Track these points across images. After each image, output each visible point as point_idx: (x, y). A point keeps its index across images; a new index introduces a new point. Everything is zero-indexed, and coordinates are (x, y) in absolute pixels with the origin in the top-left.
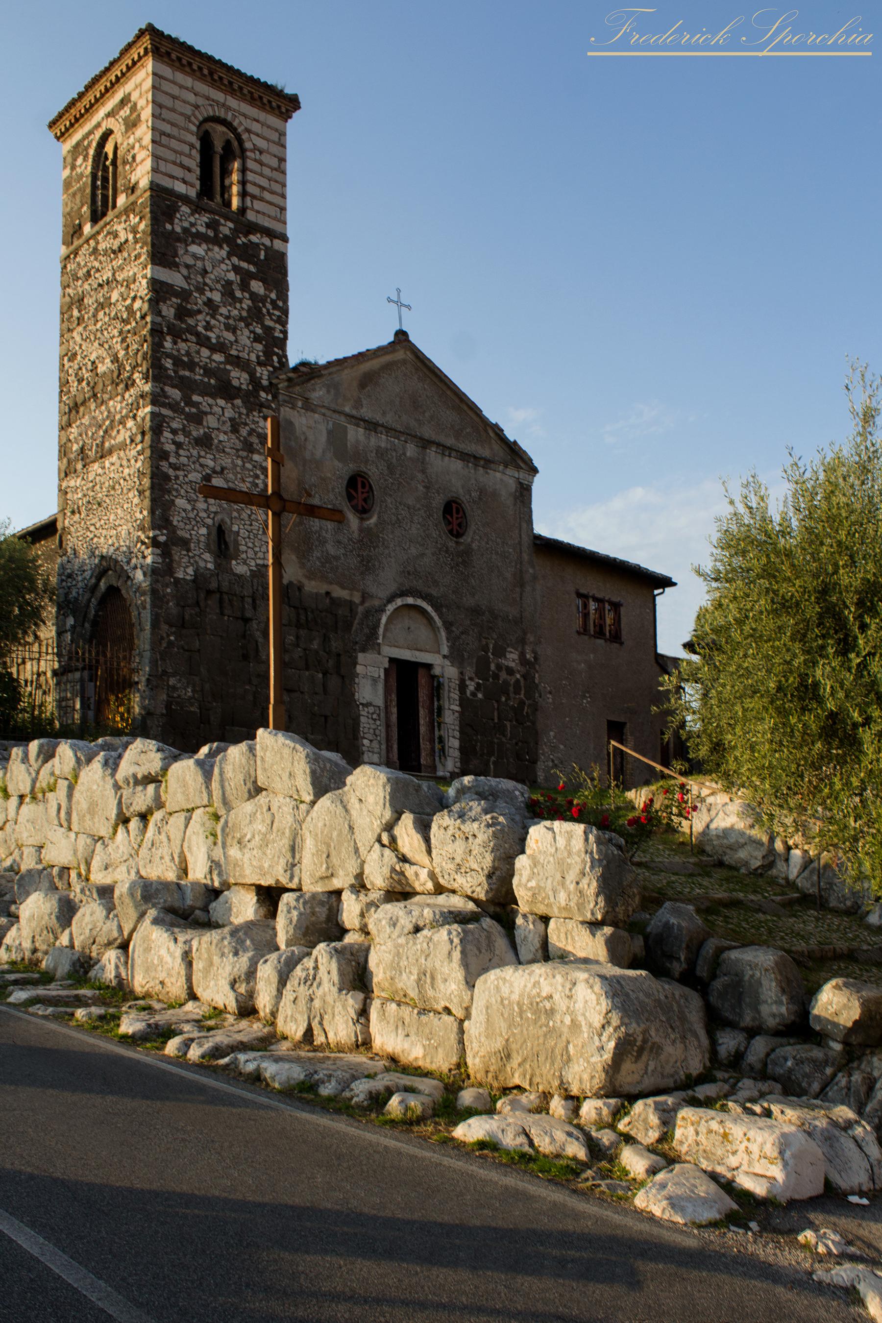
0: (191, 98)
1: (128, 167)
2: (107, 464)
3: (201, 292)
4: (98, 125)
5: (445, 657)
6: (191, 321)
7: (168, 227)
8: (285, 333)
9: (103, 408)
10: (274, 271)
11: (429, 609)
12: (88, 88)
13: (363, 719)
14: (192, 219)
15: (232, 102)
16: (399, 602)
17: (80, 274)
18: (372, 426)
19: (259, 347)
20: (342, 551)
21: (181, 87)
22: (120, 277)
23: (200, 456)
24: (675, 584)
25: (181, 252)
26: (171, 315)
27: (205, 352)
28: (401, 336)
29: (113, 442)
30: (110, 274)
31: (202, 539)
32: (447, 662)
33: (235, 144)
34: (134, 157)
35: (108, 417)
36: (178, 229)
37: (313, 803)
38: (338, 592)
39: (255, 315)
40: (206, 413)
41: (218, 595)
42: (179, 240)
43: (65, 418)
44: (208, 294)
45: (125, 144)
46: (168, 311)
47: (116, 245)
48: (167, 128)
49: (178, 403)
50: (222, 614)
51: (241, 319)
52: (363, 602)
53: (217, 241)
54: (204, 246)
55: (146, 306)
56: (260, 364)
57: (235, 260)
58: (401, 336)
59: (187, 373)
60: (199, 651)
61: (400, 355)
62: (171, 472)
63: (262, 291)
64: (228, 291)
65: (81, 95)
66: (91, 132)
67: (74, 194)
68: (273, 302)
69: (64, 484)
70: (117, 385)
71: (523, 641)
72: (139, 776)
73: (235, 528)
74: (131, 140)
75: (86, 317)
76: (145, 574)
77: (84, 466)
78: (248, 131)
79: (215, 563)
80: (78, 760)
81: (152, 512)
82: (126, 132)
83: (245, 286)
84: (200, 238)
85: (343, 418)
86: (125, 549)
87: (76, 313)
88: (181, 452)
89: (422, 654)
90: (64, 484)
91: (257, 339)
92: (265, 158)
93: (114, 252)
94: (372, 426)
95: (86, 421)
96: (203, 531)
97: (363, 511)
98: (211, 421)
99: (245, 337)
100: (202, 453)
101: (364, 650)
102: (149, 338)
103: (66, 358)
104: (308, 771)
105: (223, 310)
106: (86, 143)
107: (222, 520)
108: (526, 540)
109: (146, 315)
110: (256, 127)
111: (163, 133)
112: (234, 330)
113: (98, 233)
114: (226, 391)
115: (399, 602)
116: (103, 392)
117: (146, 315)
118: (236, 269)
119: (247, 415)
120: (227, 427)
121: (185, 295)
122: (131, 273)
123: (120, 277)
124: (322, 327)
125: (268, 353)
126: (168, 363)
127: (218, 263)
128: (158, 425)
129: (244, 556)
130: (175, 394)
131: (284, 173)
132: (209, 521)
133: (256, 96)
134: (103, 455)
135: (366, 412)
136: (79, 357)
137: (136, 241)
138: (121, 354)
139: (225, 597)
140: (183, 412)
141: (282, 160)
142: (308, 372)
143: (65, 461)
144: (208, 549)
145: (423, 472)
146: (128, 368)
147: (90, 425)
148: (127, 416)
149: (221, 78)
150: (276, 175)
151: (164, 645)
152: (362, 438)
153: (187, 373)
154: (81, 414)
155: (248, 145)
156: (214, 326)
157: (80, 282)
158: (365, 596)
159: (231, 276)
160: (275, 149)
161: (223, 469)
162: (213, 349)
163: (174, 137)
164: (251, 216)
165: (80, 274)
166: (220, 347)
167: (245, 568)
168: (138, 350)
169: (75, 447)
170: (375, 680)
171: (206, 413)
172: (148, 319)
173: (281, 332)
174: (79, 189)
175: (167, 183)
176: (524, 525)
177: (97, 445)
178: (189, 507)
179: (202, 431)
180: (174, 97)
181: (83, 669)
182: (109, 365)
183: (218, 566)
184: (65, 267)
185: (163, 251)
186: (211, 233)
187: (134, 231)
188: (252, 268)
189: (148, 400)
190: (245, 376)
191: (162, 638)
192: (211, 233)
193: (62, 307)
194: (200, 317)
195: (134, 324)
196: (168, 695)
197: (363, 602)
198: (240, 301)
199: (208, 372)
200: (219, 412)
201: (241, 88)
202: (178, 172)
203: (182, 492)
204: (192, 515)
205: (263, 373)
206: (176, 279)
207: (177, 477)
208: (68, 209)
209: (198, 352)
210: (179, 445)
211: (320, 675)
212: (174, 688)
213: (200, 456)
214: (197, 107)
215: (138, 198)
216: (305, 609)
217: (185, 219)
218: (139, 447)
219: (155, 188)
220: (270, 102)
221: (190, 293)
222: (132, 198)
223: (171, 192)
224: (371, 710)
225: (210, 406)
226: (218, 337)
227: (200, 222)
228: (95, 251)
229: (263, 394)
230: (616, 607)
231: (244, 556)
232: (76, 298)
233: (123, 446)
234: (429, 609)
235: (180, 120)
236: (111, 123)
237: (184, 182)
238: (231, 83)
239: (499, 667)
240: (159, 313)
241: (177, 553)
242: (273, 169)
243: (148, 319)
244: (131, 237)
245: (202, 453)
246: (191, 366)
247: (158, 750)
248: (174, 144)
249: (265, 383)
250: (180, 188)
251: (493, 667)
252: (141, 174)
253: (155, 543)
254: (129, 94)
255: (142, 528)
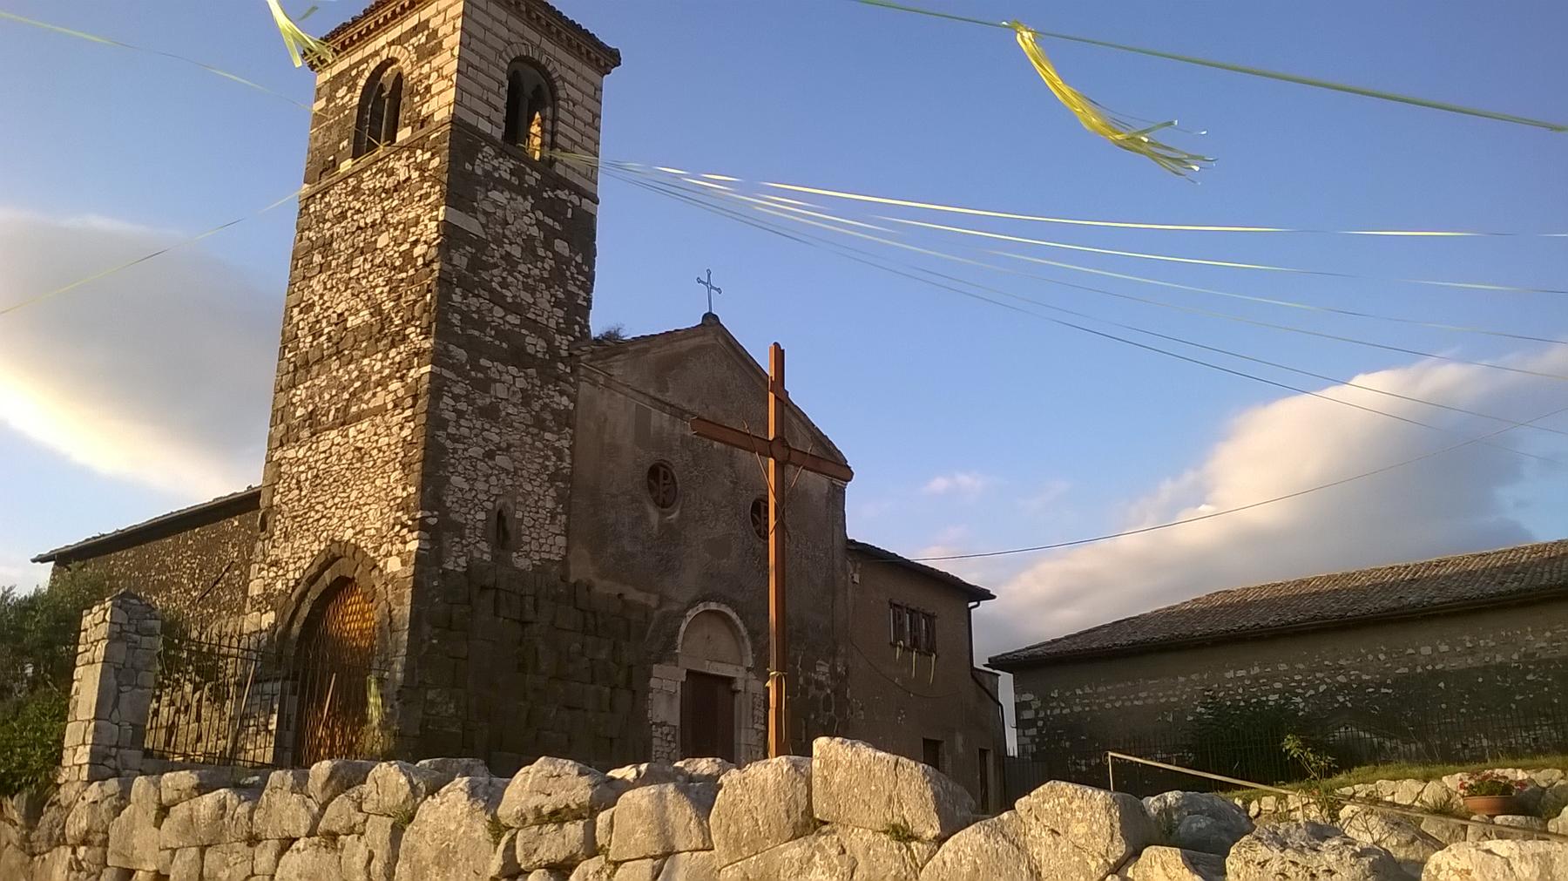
0: (504, 32)
1: (417, 99)
2: (352, 432)
3: (500, 245)
4: (377, 53)
5: (748, 669)
6: (484, 275)
7: (468, 166)
8: (589, 301)
9: (352, 366)
10: (582, 232)
11: (734, 616)
12: (367, 13)
13: (655, 741)
14: (495, 163)
15: (548, 46)
16: (701, 607)
17: (329, 215)
18: (678, 413)
19: (560, 313)
20: (639, 548)
21: (494, 19)
22: (393, 219)
23: (483, 430)
24: (993, 597)
25: (480, 197)
26: (463, 263)
27: (498, 312)
28: (710, 319)
29: (364, 406)
30: (378, 216)
31: (479, 525)
32: (751, 676)
33: (546, 90)
34: (428, 88)
35: (358, 378)
36: (479, 172)
37: (940, 840)
38: (633, 595)
39: (557, 276)
40: (495, 381)
41: (492, 593)
42: (479, 183)
43: (286, 378)
44: (508, 248)
45: (416, 74)
46: (460, 260)
47: (390, 183)
48: (476, 60)
49: (463, 366)
50: (496, 614)
51: (542, 280)
52: (659, 607)
53: (522, 191)
54: (507, 194)
55: (433, 252)
56: (559, 331)
57: (540, 214)
58: (710, 319)
59: (476, 333)
60: (467, 658)
61: (709, 340)
62: (448, 444)
63: (566, 253)
64: (529, 246)
65: (355, 21)
66: (365, 60)
67: (329, 128)
68: (578, 266)
69: (277, 455)
70: (378, 340)
71: (833, 653)
72: (545, 811)
73: (519, 515)
74: (426, 69)
75: (334, 263)
76: (404, 563)
77: (313, 434)
78: (564, 80)
79: (492, 553)
80: (414, 788)
81: (422, 489)
82: (419, 60)
83: (548, 245)
84: (502, 185)
85: (647, 401)
86: (373, 532)
87: (317, 259)
88: (462, 422)
89: (719, 665)
90: (277, 455)
91: (558, 304)
92: (578, 110)
93: (386, 191)
94: (678, 413)
95: (322, 381)
96: (482, 516)
97: (663, 505)
98: (500, 390)
99: (544, 299)
100: (487, 426)
101: (659, 661)
102: (434, 288)
103: (296, 310)
104: (929, 794)
105: (522, 268)
106: (354, 73)
107: (504, 504)
108: (838, 543)
109: (432, 261)
110: (570, 76)
111: (470, 65)
112: (532, 290)
113: (363, 170)
114: (518, 357)
115: (701, 607)
116: (352, 348)
117: (432, 261)
118: (539, 224)
119: (541, 387)
120: (517, 399)
121: (481, 245)
122: (412, 215)
123: (393, 219)
124: (633, 295)
125: (570, 322)
126: (456, 319)
127: (523, 217)
128: (437, 386)
129: (527, 548)
130: (461, 354)
131: (598, 129)
132: (489, 505)
133: (574, 43)
134: (345, 420)
135: (669, 397)
136: (317, 309)
137: (423, 179)
138: (388, 305)
139: (502, 594)
140: (466, 376)
141: (597, 116)
142: (612, 344)
143: (282, 427)
144: (485, 538)
145: (731, 466)
146: (397, 321)
147: (327, 387)
148: (390, 377)
149: (538, 18)
150: (589, 130)
151: (425, 649)
152: (666, 424)
153: (476, 333)
154: (314, 373)
155: (562, 94)
156: (511, 284)
157: (328, 225)
158: (663, 600)
159: (534, 231)
160: (589, 103)
161: (509, 446)
162: (508, 309)
163: (481, 71)
164: (559, 169)
165: (329, 215)
166: (516, 308)
167: (528, 562)
168: (416, 302)
169: (300, 412)
170: (671, 696)
171: (495, 381)
172: (436, 266)
173: (585, 299)
174: (338, 122)
175: (471, 119)
176: (837, 529)
177: (337, 410)
178: (466, 487)
179: (488, 401)
180: (486, 29)
181: (286, 679)
182: (367, 318)
183: (495, 558)
184: (307, 207)
185: (459, 190)
186: (515, 180)
187: (421, 168)
188: (557, 227)
189: (427, 357)
190: (542, 343)
191: (423, 641)
192: (515, 180)
193: (295, 252)
194: (495, 272)
195: (412, 272)
196: (425, 713)
197: (659, 607)
198: (543, 259)
199: (500, 334)
200: (509, 381)
201: (559, 32)
202: (484, 109)
203: (460, 468)
204: (469, 496)
205: (562, 342)
206: (473, 226)
207: (455, 451)
208: (318, 144)
209: (491, 310)
210: (460, 414)
211: (607, 690)
212: (433, 703)
213: (483, 430)
214: (510, 43)
215: (432, 132)
216: (594, 613)
217: (487, 161)
218: (408, 413)
219: (455, 120)
220: (588, 53)
221: (487, 243)
222: (421, 133)
223: (474, 130)
224: (666, 730)
225: (500, 373)
226: (514, 297)
227: (504, 167)
228: (356, 191)
229: (561, 366)
230: (930, 618)
231: (527, 548)
232: (320, 242)
233: (381, 410)
234: (734, 616)
235: (491, 55)
236: (395, 51)
237: (490, 121)
238: (548, 25)
239: (808, 681)
240: (449, 261)
241: (449, 540)
242: (586, 124)
243: (436, 266)
244: (415, 175)
245: (487, 426)
246: (482, 325)
247: (580, 774)
248: (481, 77)
249: (564, 353)
250: (485, 127)
251: (801, 680)
252: (440, 105)
253: (422, 525)
254: (428, 21)
255: (403, 506)
